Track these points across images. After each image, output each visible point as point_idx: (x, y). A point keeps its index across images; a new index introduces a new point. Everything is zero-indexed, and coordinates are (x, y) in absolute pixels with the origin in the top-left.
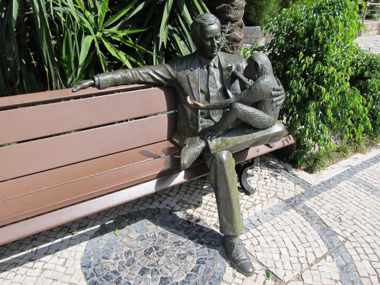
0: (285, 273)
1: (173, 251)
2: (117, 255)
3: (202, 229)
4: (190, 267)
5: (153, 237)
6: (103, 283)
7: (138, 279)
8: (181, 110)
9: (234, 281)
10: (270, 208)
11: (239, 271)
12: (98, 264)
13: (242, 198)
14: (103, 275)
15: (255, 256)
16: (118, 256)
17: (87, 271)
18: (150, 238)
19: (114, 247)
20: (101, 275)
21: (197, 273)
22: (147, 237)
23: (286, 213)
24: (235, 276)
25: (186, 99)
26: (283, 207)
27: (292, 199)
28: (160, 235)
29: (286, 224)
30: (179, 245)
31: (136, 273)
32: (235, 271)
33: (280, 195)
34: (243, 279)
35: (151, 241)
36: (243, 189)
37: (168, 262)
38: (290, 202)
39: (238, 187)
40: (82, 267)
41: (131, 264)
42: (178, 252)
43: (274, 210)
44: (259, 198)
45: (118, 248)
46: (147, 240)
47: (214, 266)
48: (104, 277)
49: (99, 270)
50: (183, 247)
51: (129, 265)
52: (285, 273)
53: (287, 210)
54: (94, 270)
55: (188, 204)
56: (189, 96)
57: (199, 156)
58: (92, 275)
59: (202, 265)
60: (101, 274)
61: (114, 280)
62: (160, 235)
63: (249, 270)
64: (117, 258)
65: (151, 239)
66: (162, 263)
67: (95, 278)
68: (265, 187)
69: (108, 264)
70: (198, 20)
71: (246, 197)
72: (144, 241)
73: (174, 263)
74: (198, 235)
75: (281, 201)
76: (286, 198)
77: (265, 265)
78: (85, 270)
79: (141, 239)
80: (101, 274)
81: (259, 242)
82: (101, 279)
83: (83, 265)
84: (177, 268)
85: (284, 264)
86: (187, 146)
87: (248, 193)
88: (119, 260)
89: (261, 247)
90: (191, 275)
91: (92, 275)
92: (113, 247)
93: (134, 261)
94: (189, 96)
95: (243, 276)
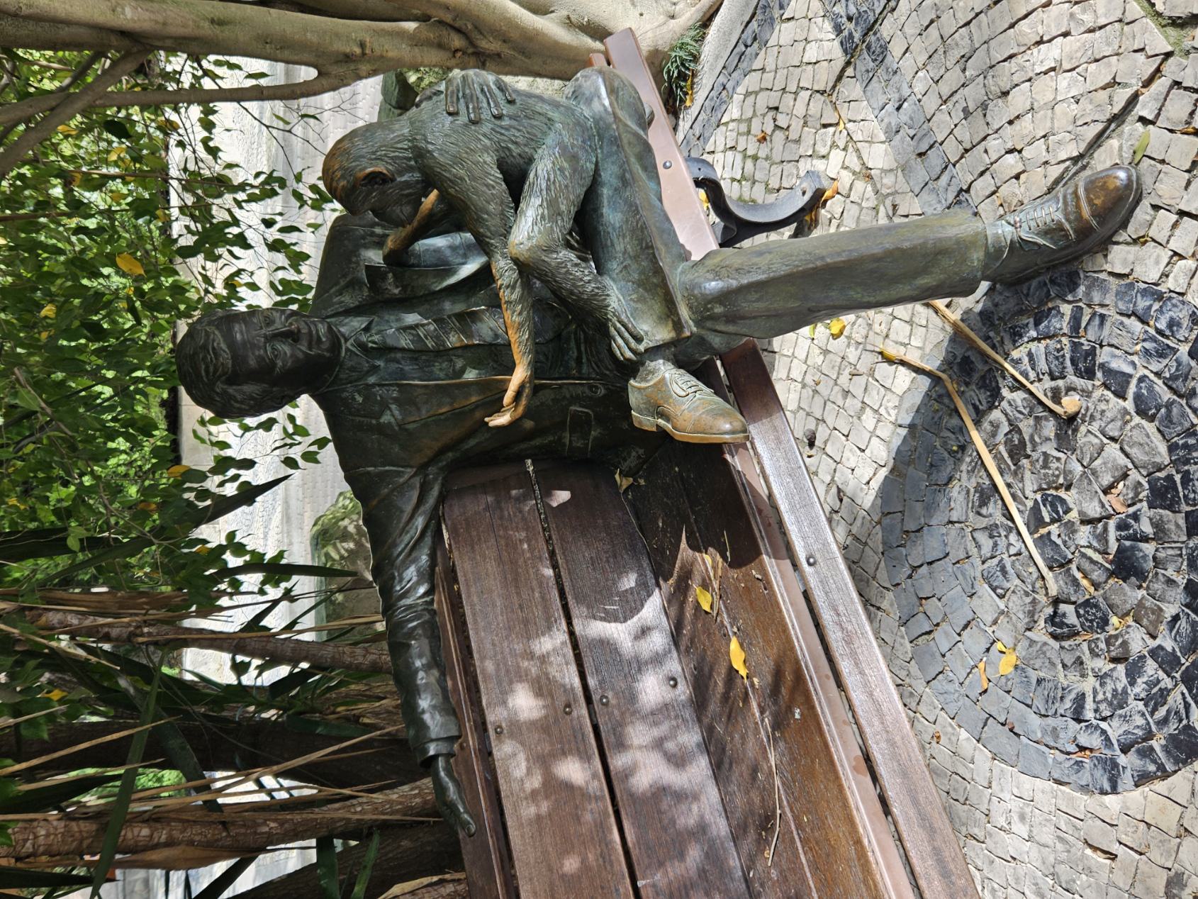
0: (1135, 51)
1: (1045, 466)
2: (1064, 666)
3: (958, 360)
4: (1107, 401)
5: (991, 537)
6: (1176, 713)
7: (1158, 586)
8: (523, 446)
9: (1162, 238)
10: (876, 112)
11: (1119, 218)
12: (1104, 732)
13: (837, 216)
14: (1143, 715)
15: (1063, 166)
16: (1069, 662)
17: (1129, 772)
18: (995, 545)
19: (1034, 676)
20: (1144, 722)
21: (1131, 376)
22: (992, 557)
23: (896, 49)
24: (1138, 241)
25: (498, 428)
26: (871, 65)
27: (838, 29)
28: (984, 511)
29: (941, 51)
30: (1022, 443)
31: (1132, 594)
32: (1122, 236)
33: (824, 77)
34: (1156, 208)
35: (1010, 544)
36: (804, 219)
37: (1090, 482)
38: (851, 36)
39: (796, 235)
40: (1114, 790)
41: (1099, 615)
42: (1050, 448)
43: (883, 99)
44: (837, 156)
45: (1038, 663)
46: (1005, 556)
47: (1103, 317)
48: (1152, 714)
49: (1125, 727)
50: (1026, 426)
51: (1105, 622)
52: (1135, 51)
53: (884, 48)
54: (1125, 750)
55: (863, 409)
56: (487, 419)
57: (698, 379)
58: (1147, 753)
59: (1099, 360)
60: (1140, 721)
61: (1161, 674)
62: (984, 511)
63: (1118, 183)
64: (1079, 662)
65: (1002, 542)
66: (1096, 503)
67: (1157, 744)
68: (793, 135)
69: (1100, 697)
70: (979, 274)
71: (834, 206)
72: (1009, 568)
73: (1092, 460)
74: (983, 378)
75: (850, 72)
76: (839, 57)
77: (1100, 127)
78: (1127, 780)
79: (1001, 577)
80: (1140, 721)
81: (1010, 151)
82: (1158, 723)
83: (1107, 786)
84: (1112, 450)
85: (1098, 57)
86: (661, 422)
87: (818, 200)
88: (1086, 657)
89: (1030, 144)
90: (1138, 398)
91: (1147, 753)
92: (1034, 682)
93: (1087, 603)
94: (487, 419)
95: (1145, 204)
